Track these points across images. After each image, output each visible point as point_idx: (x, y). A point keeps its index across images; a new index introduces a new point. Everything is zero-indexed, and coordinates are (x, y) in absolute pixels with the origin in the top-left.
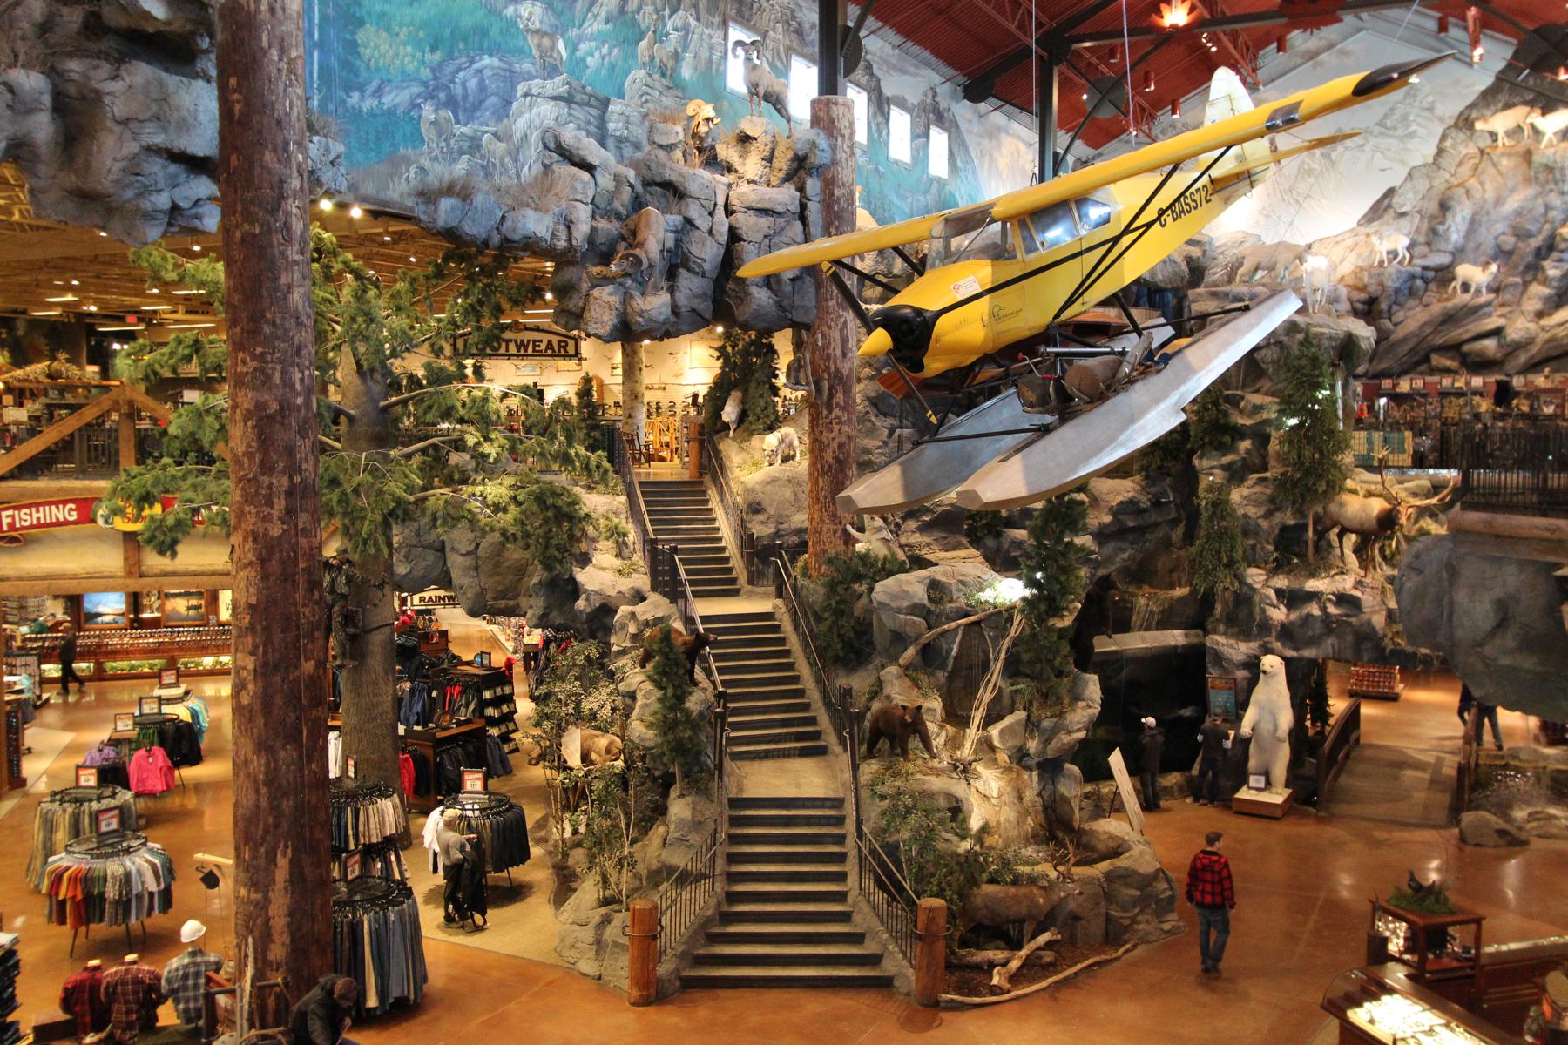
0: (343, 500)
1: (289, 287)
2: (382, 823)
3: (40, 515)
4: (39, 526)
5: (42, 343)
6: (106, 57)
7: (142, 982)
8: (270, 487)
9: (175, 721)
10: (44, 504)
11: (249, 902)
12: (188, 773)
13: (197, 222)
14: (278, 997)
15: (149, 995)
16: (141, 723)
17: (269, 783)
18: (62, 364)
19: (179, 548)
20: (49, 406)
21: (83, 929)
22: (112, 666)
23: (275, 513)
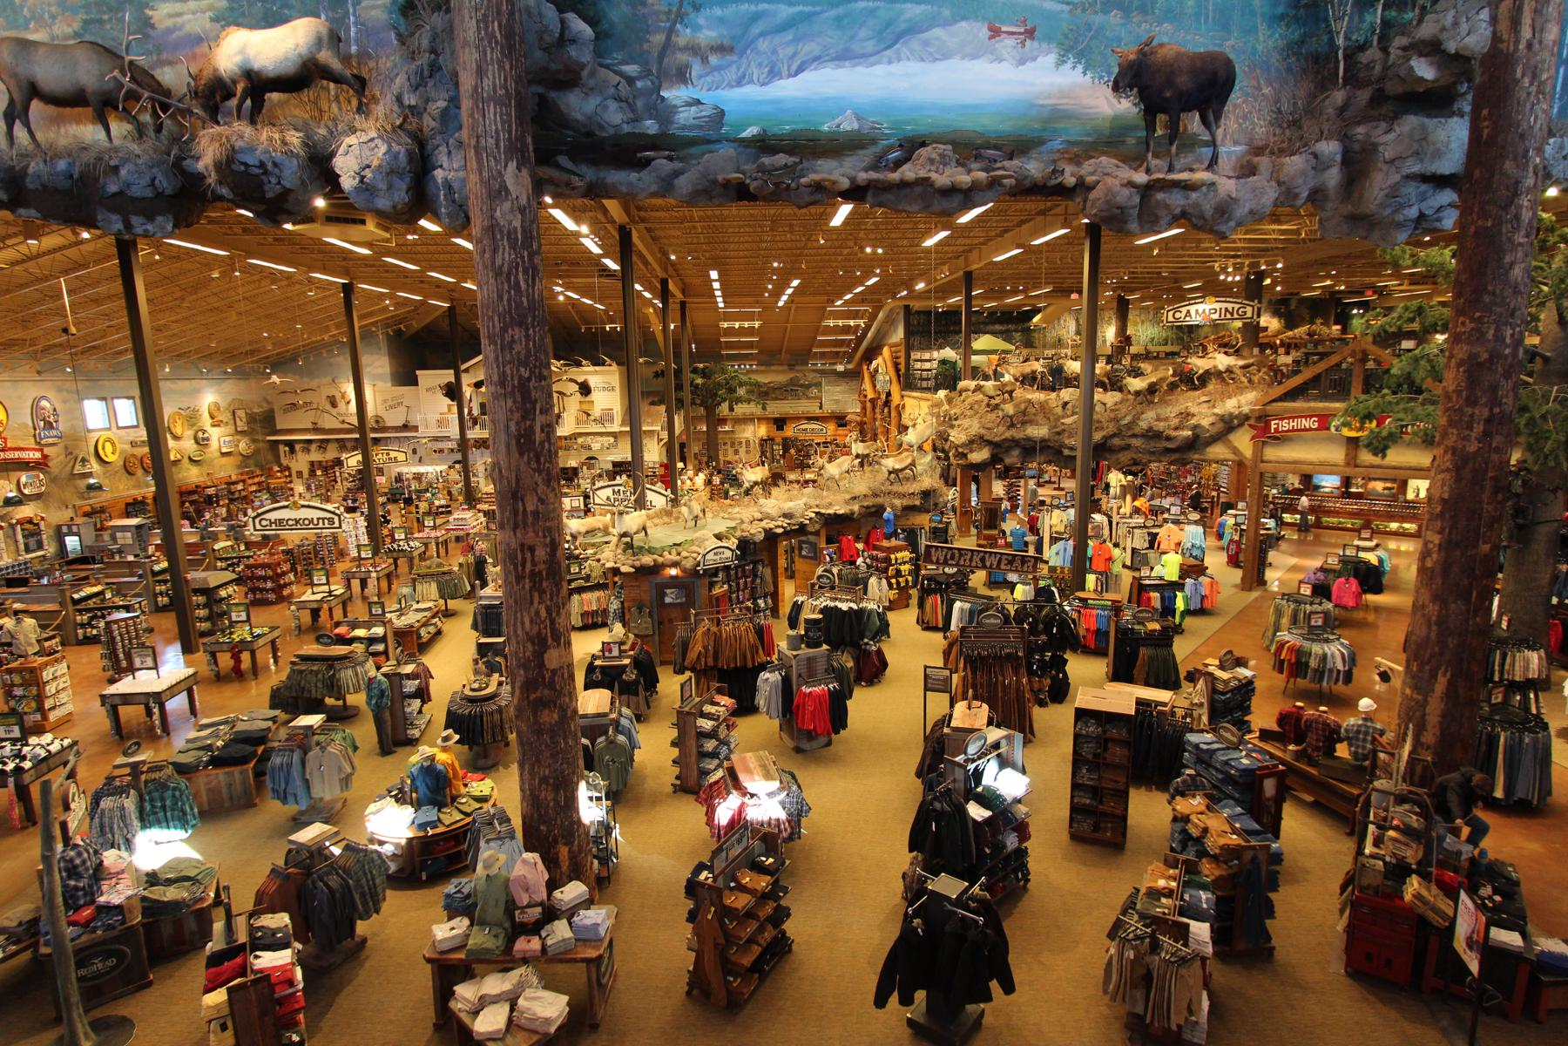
0: (1531, 422)
1: (1512, 265)
2: (1526, 668)
3: (1294, 424)
4: (1293, 430)
5: (1305, 313)
6: (1385, 118)
7: (1329, 725)
8: (1472, 416)
9: (1367, 563)
10: (1297, 417)
11: (1412, 699)
12: (1371, 598)
13: (1437, 225)
14: (1425, 768)
15: (1332, 735)
16: (1344, 560)
17: (1438, 624)
18: (1318, 327)
19: (1389, 452)
20: (1306, 354)
21: (1292, 680)
22: (1326, 520)
23: (1473, 435)
